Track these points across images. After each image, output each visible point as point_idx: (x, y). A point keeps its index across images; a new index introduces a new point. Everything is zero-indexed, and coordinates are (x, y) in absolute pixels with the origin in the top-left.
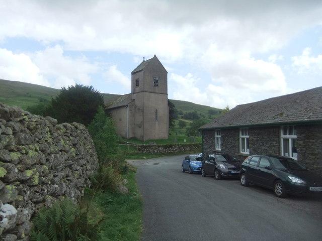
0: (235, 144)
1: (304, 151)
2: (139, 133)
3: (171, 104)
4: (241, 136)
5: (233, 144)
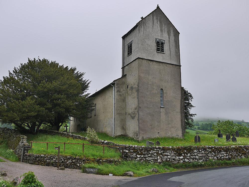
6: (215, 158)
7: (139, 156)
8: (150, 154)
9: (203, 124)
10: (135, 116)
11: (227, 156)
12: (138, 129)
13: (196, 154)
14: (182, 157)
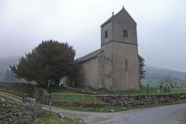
11: (164, 99)
12: (112, 84)
13: (147, 99)
14: (138, 101)
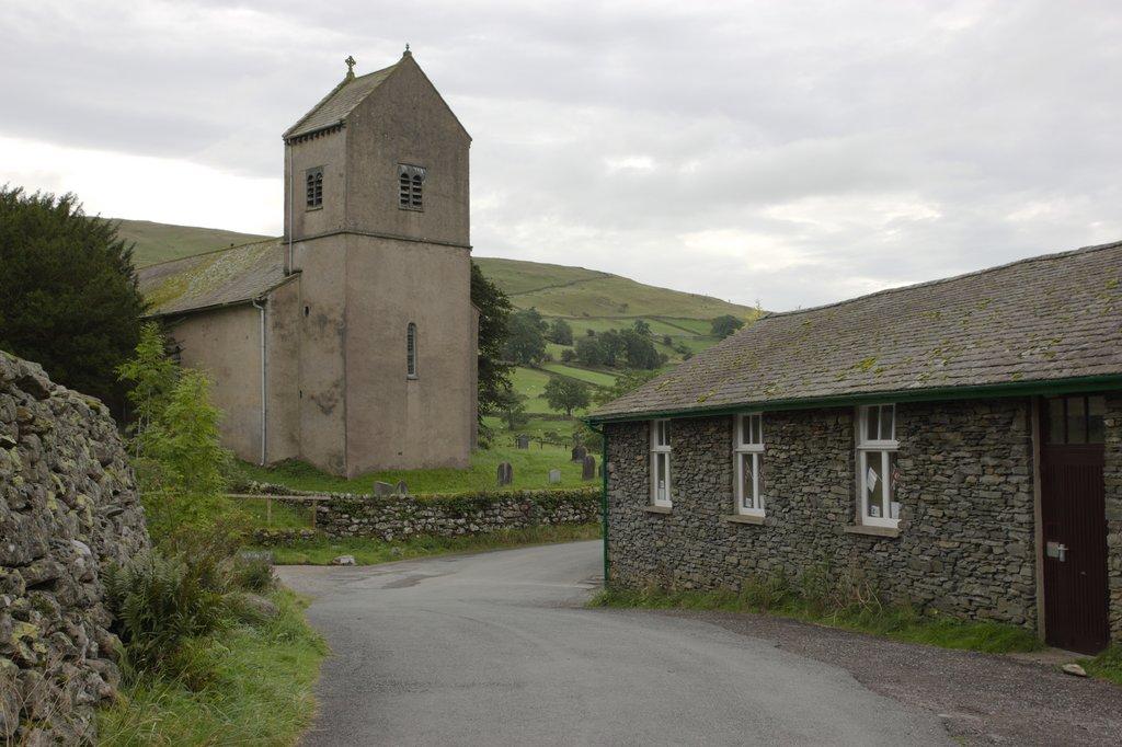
0: (718, 477)
1: (916, 495)
2: (323, 438)
3: (484, 289)
4: (742, 447)
5: (713, 480)
6: (545, 520)
7: (357, 521)
8: (384, 514)
9: (591, 333)
10: (334, 406)
11: (576, 514)
12: (343, 444)
13: (497, 512)
